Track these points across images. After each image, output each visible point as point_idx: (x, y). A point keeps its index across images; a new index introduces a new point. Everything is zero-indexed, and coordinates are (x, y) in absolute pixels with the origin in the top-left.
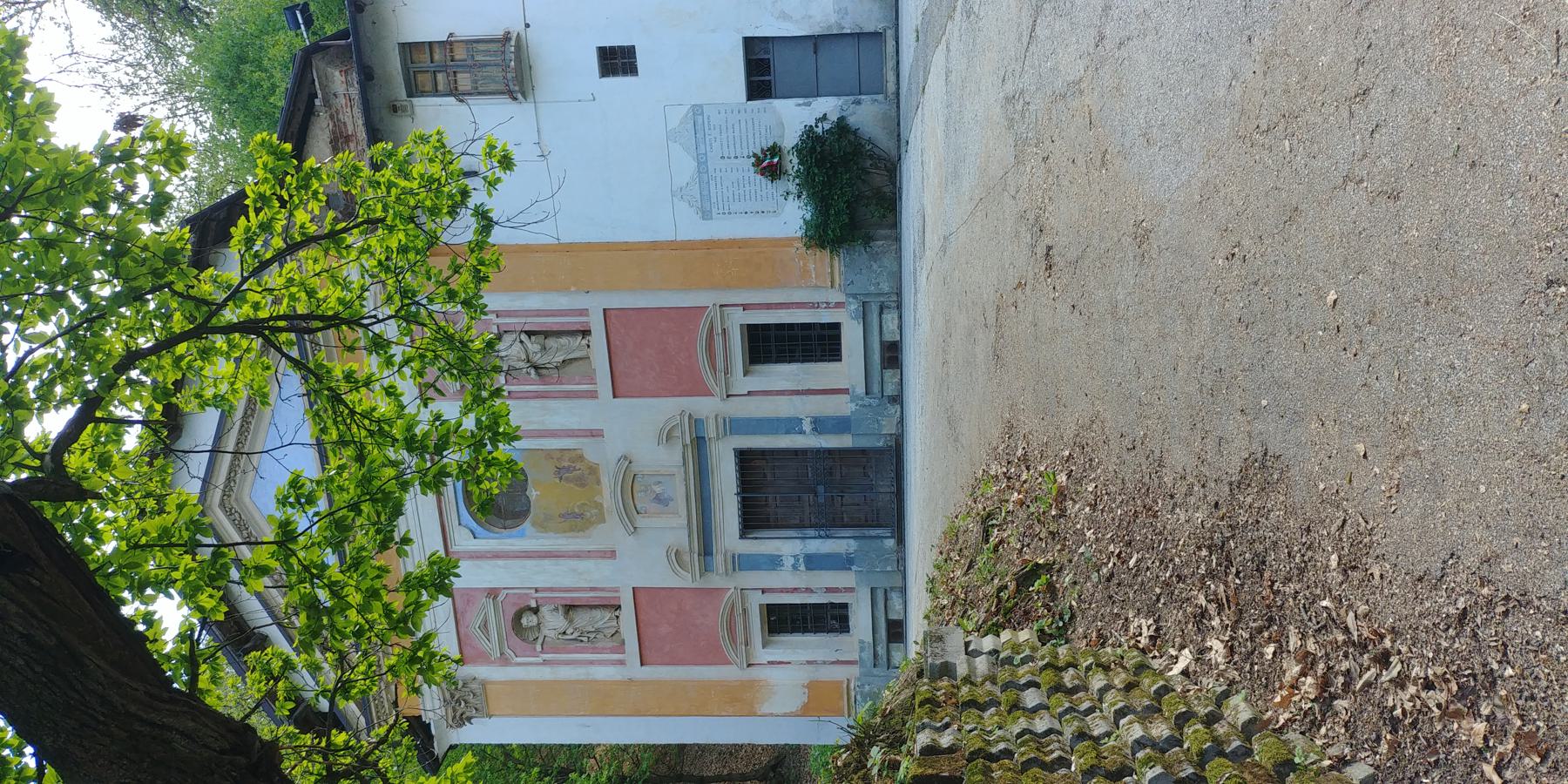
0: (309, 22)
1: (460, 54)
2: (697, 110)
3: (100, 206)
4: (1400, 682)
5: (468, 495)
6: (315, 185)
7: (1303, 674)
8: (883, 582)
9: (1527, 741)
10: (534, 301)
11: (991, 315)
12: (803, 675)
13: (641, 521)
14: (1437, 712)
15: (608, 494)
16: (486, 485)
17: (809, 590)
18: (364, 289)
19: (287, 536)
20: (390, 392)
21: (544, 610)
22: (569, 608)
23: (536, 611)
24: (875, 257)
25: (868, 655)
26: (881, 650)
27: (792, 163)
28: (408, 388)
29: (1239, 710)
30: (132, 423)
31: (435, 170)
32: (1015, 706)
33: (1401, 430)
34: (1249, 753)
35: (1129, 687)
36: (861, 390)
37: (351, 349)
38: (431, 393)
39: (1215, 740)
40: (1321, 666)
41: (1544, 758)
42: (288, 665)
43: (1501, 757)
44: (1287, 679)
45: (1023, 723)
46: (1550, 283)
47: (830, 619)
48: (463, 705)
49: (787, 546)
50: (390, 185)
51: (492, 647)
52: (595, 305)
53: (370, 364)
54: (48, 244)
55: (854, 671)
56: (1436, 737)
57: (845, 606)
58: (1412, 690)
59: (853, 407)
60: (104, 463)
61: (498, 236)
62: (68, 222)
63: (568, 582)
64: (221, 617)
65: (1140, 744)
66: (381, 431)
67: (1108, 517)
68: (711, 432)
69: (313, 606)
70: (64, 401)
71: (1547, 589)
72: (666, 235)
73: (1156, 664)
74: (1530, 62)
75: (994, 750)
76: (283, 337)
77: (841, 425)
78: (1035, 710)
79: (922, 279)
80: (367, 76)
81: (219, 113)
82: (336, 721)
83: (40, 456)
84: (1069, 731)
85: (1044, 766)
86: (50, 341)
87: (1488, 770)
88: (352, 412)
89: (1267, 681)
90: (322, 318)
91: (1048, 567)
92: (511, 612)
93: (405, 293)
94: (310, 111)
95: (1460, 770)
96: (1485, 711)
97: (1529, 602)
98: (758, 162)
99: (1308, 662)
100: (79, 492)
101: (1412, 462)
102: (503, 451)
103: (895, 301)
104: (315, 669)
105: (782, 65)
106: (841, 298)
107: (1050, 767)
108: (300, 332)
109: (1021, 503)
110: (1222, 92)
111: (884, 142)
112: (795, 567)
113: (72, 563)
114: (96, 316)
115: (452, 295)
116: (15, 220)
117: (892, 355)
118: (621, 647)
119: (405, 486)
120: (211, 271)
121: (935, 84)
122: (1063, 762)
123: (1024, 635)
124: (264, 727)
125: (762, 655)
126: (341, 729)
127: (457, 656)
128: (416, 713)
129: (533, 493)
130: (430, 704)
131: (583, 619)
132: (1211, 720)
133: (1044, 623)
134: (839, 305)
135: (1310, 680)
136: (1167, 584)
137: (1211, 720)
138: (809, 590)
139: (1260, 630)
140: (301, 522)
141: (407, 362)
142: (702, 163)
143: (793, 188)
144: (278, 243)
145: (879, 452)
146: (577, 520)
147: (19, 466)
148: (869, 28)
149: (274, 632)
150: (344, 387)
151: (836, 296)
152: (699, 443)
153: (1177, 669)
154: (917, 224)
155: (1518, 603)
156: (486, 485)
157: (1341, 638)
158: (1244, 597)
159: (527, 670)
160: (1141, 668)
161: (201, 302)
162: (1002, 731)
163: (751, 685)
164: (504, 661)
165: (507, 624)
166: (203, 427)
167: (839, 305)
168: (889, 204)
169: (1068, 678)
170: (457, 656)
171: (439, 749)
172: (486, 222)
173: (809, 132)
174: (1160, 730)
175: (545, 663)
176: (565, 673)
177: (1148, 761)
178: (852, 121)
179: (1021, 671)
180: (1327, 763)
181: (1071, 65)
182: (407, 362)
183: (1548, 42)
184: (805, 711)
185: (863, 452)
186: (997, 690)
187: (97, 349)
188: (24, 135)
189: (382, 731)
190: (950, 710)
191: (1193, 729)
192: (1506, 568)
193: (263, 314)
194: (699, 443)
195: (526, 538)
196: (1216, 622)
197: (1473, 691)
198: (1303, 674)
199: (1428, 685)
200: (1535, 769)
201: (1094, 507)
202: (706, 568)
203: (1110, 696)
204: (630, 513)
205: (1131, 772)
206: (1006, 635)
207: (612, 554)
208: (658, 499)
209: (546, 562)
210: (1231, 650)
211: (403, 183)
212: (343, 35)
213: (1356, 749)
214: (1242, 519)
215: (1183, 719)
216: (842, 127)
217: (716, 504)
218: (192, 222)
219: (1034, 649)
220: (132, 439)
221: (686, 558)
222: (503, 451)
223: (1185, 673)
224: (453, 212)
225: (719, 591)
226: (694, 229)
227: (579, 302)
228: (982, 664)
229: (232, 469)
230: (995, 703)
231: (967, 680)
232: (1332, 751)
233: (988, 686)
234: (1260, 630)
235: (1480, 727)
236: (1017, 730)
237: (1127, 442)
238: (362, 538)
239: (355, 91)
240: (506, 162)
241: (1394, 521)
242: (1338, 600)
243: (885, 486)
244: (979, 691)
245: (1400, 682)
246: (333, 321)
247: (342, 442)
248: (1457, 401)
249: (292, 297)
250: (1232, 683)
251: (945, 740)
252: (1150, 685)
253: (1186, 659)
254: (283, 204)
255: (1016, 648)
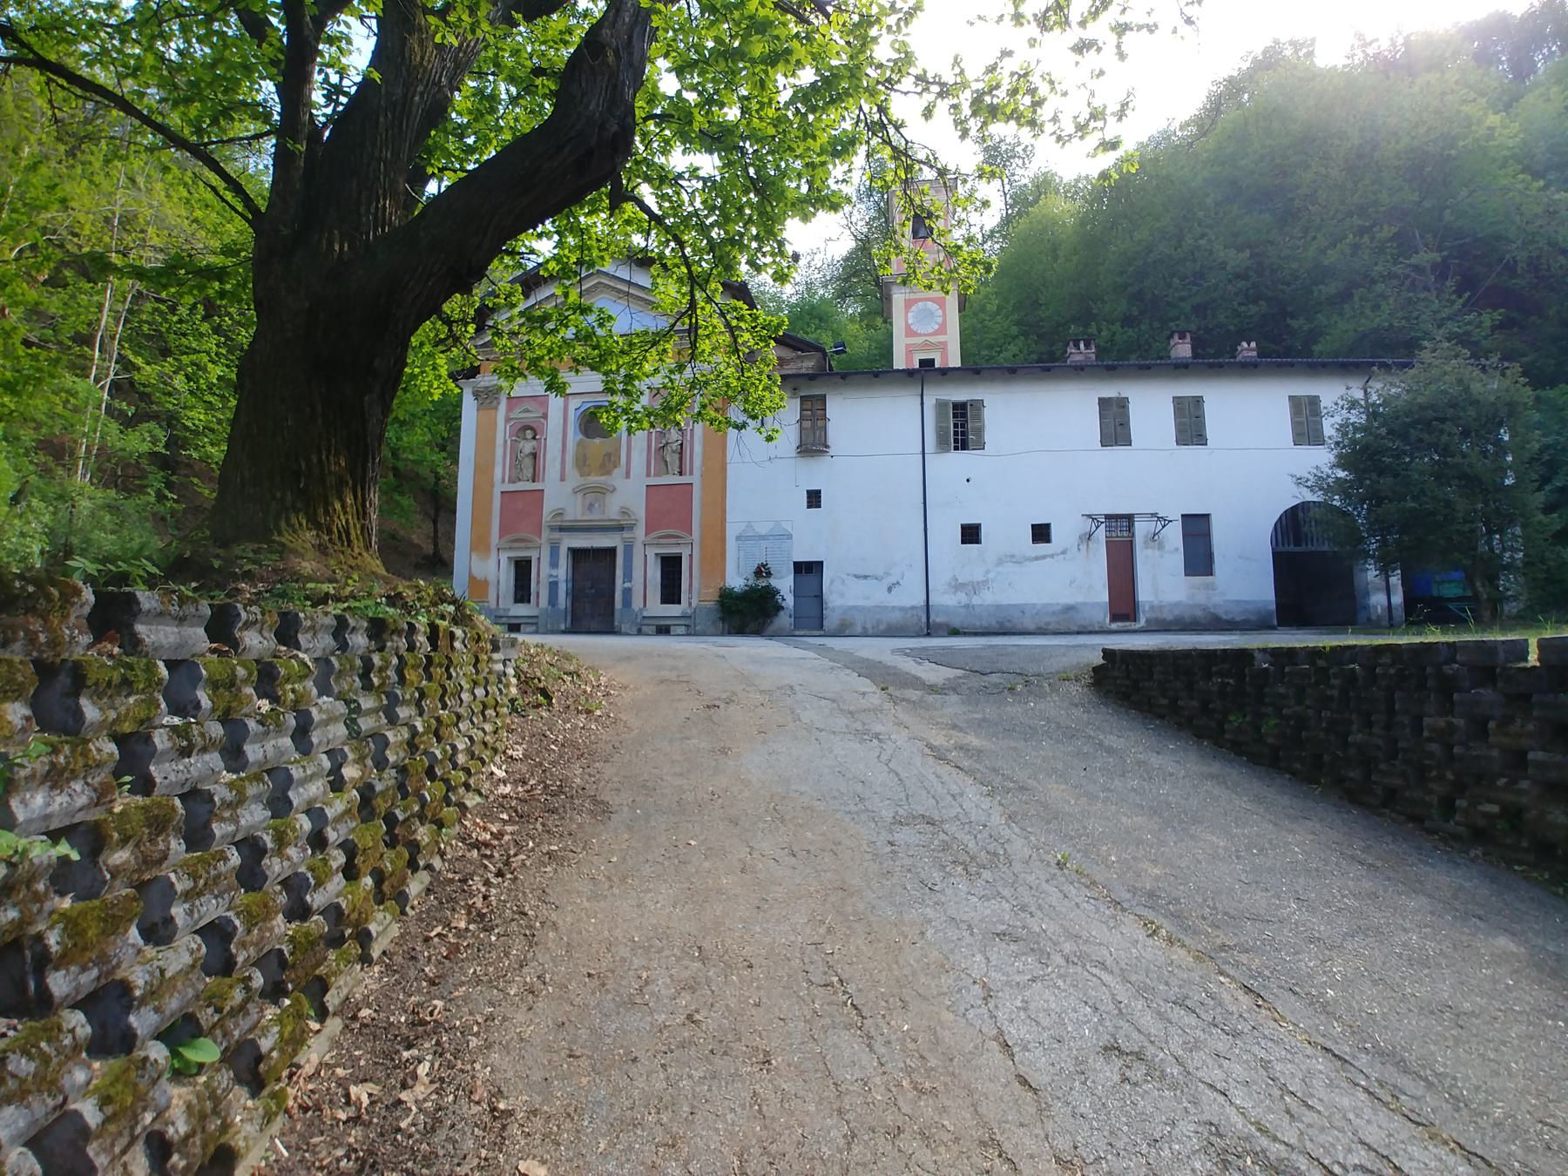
0: (837, 352)
1: (820, 423)
2: (790, 537)
3: (757, 238)
4: (487, 883)
5: (600, 407)
6: (762, 344)
7: (492, 833)
8: (541, 621)
9: (454, 949)
10: (698, 448)
11: (685, 679)
12: (492, 578)
13: (580, 496)
14: (471, 902)
15: (595, 479)
16: (605, 415)
17: (538, 583)
18: (709, 363)
19: (585, 310)
20: (656, 371)
21: (534, 442)
22: (534, 456)
23: (534, 438)
24: (714, 623)
25: (501, 613)
26: (504, 620)
27: (762, 583)
28: (657, 381)
29: (472, 801)
30: (647, 240)
31: (767, 403)
32: (475, 683)
33: (623, 880)
34: (448, 805)
35: (485, 744)
36: (645, 614)
37: (679, 353)
38: (655, 392)
39: (456, 787)
40: (496, 843)
41: (446, 957)
42: (514, 306)
43: (446, 936)
44: (489, 825)
45: (466, 686)
46: (700, 948)
47: (522, 592)
48: (487, 398)
49: (563, 572)
50: (760, 381)
51: (515, 414)
52: (695, 479)
53: (670, 361)
54: (740, 210)
55: (493, 605)
56: (457, 903)
57: (529, 601)
58: (483, 889)
59: (636, 609)
60: (628, 222)
61: (732, 432)
62: (750, 220)
63: (548, 457)
64: (541, 273)
65: (454, 747)
66: (634, 364)
67: (578, 735)
68: (626, 534)
69: (545, 318)
70: (660, 207)
71: (539, 956)
72: (730, 516)
73: (497, 759)
74: (808, 932)
75: (452, 670)
76: (687, 321)
77: (627, 602)
78: (473, 694)
79: (702, 645)
80: (811, 377)
81: (797, 305)
82: (480, 330)
83: (632, 191)
84: (461, 711)
85: (443, 696)
86: (692, 204)
87: (439, 929)
88: (646, 351)
89: (487, 814)
90: (695, 341)
91: (550, 704)
92: (534, 425)
93: (706, 383)
94: (796, 349)
95: (438, 915)
96: (472, 927)
97: (531, 947)
98: (764, 566)
99: (498, 836)
100: (614, 207)
101: (606, 886)
102: (622, 424)
103: (691, 632)
104: (510, 320)
105: (809, 579)
106: (694, 605)
107: (442, 699)
108: (689, 331)
109: (585, 692)
110: (794, 787)
111: (772, 628)
112: (551, 576)
113: (576, 198)
114: (704, 230)
115: (704, 406)
116: (752, 195)
117: (663, 630)
118: (511, 481)
119: (606, 374)
120: (721, 289)
121: (799, 653)
122: (444, 707)
123: (514, 691)
124: (479, 291)
125: (504, 557)
126: (477, 331)
127: (512, 395)
128: (482, 371)
129: (597, 441)
130: (485, 380)
131: (528, 462)
132: (467, 786)
133: (521, 701)
134: (690, 604)
135: (488, 837)
136: (541, 764)
137: (467, 786)
138: (538, 583)
139: (516, 811)
140: (592, 318)
141: (671, 380)
142: (763, 537)
143: (750, 583)
144: (734, 323)
145: (613, 623)
146: (582, 463)
147: (629, 180)
148: (825, 623)
149: (532, 301)
150: (660, 348)
151: (695, 603)
152: (621, 528)
153: (494, 769)
154: (731, 644)
155: (531, 940)
156: (605, 415)
157: (512, 852)
158: (534, 804)
159: (502, 431)
160: (495, 751)
161: (707, 281)
162: (463, 674)
163: (488, 550)
164: (508, 420)
165: (526, 422)
166: (643, 279)
167: (690, 604)
168: (740, 631)
169: (490, 712)
170: (512, 395)
171: (462, 382)
172: (740, 427)
173: (778, 592)
174: (461, 759)
175: (506, 442)
176: (499, 452)
177: (444, 751)
178: (782, 613)
179: (495, 688)
180: (442, 846)
181: (806, 717)
182: (671, 380)
183: (816, 939)
184: (472, 578)
185: (613, 614)
186: (484, 674)
187: (686, 227)
188: (793, 205)
189: (473, 351)
190: (474, 649)
191: (462, 776)
192: (551, 934)
193: (699, 312)
194: (621, 528)
195: (574, 435)
196: (520, 789)
197: (482, 921)
198: (492, 833)
199: (485, 897)
200: (440, 953)
201: (583, 728)
202: (552, 529)
203: (480, 733)
204: (584, 490)
205: (439, 741)
206: (514, 681)
207: (562, 479)
208: (591, 506)
209: (560, 445)
210: (504, 797)
211: (761, 388)
212: (831, 368)
213: (450, 861)
214: (576, 801)
215: (467, 771)
216: (780, 608)
217: (588, 535)
218: (744, 285)
219: (506, 695)
220: (638, 240)
221: (558, 518)
222: (622, 424)
223: (492, 773)
224: (745, 410)
225: (540, 536)
226: (732, 531)
227: (697, 471)
228: (499, 667)
229: (619, 291)
230: (477, 672)
231: (490, 659)
232: (448, 848)
233: (487, 670)
234: (516, 811)
235: (463, 925)
236: (463, 683)
237: (617, 744)
238: (579, 350)
239: (803, 371)
240: (769, 439)
241: (575, 877)
242: (533, 850)
243: (594, 626)
244: (484, 664)
245: (487, 883)
246: (694, 345)
247: (631, 345)
248: (639, 906)
249: (707, 327)
250: (487, 797)
251: (457, 644)
252: (486, 755)
253: (500, 774)
254: (753, 328)
255: (507, 686)
